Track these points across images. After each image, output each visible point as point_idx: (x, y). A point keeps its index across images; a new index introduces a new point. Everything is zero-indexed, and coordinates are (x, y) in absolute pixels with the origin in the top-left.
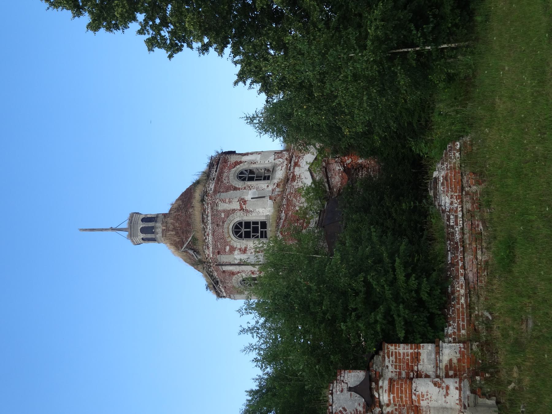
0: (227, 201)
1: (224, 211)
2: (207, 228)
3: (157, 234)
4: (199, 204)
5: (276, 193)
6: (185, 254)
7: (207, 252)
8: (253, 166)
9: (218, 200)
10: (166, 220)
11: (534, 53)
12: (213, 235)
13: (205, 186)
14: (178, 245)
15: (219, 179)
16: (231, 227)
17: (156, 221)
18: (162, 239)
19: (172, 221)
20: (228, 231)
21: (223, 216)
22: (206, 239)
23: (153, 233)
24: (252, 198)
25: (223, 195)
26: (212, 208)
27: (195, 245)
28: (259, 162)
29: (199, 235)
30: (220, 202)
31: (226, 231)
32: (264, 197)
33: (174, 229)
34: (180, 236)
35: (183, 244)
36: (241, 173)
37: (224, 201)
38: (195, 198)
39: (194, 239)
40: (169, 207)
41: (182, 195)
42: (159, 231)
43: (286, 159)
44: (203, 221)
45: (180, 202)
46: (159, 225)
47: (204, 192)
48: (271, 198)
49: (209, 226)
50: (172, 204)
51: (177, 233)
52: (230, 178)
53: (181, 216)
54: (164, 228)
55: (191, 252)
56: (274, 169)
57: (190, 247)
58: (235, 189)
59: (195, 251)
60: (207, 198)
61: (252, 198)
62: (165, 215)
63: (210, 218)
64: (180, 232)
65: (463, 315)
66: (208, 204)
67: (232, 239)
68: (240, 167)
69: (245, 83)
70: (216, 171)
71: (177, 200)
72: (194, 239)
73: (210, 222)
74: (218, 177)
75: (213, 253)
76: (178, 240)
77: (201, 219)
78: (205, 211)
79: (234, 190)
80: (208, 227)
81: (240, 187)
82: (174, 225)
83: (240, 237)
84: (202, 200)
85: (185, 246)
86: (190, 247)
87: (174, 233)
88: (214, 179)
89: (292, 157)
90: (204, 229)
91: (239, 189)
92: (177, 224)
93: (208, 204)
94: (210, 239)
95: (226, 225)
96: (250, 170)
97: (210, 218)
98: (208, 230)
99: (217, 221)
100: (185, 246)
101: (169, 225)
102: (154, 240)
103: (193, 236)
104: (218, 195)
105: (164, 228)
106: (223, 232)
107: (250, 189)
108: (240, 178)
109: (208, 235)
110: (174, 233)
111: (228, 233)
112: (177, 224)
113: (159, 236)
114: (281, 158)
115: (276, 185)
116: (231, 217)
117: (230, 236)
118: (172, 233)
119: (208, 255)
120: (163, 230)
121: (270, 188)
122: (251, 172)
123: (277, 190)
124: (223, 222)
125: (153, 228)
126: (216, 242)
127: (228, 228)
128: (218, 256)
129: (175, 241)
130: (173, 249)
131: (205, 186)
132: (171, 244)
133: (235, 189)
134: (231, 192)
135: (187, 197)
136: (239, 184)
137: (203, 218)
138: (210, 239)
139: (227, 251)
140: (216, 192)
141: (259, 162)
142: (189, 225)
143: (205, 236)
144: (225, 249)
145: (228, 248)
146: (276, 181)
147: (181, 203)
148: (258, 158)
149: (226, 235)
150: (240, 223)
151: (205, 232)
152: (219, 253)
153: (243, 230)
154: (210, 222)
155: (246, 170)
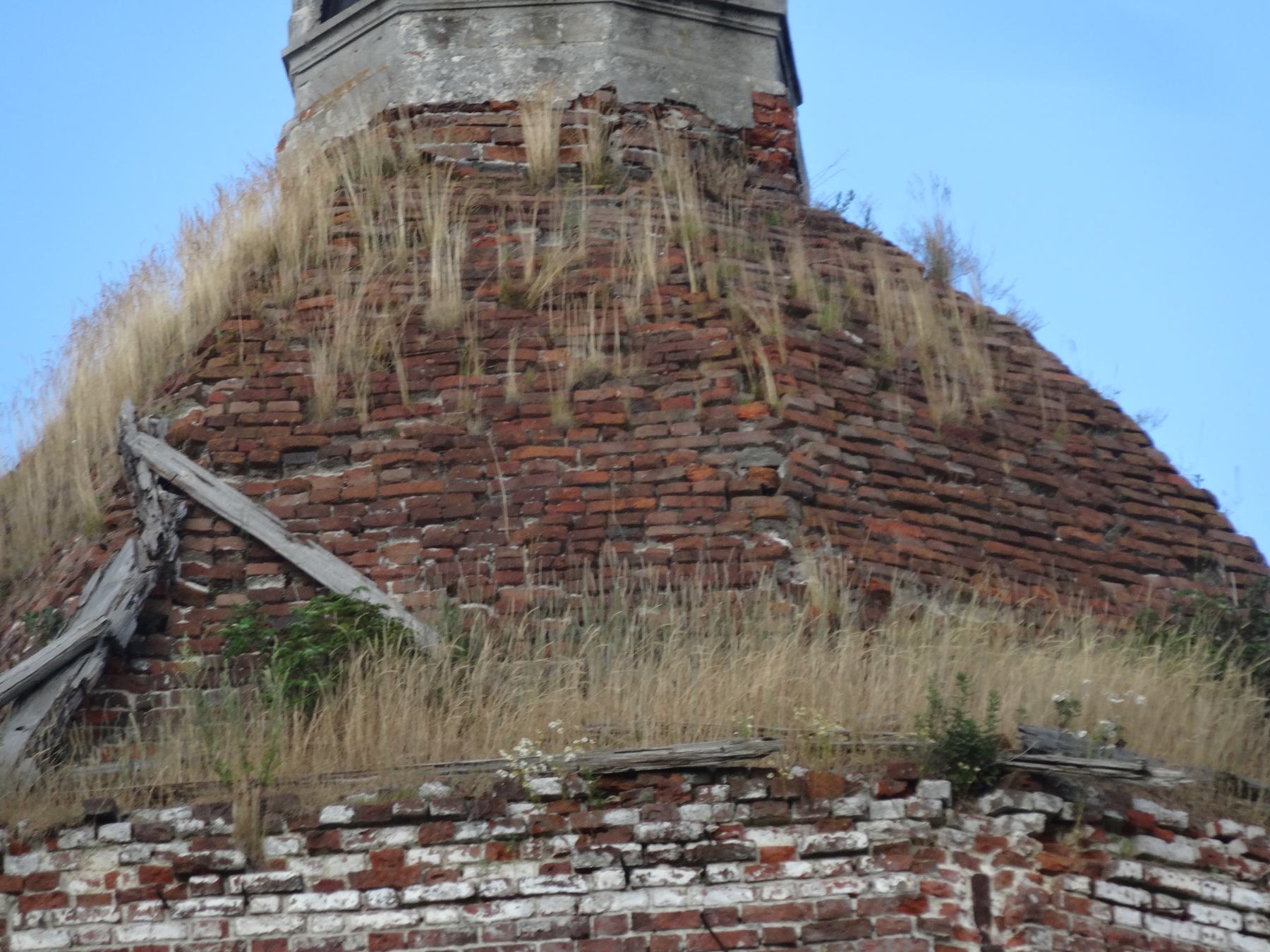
2: (504, 850)
4: (915, 701)
10: (672, 166)
13: (1235, 790)
14: (237, 375)
18: (354, 118)
19: (649, 263)
22: (321, 841)
27: (238, 657)
29: (385, 721)
33: (510, 308)
34: (383, 398)
35: (257, 467)
38: (1036, 628)
39: (318, 648)
40: (896, 221)
41: (1098, 418)
44: (614, 784)
45: (965, 389)
47: (1119, 788)
50: (938, 269)
51: (432, 354)
53: (717, 417)
54: (539, 137)
55: (108, 602)
57: (189, 579)
59: (129, 659)
60: (1017, 830)
62: (765, 145)
63: (668, 890)
64: (457, 405)
66: (913, 852)
69: (42, 554)
71: (1010, 343)
72: (318, 648)
73: (607, 894)
76: (320, 372)
77: (653, 749)
78: (795, 801)
80: (525, 874)
82: (574, 295)
84: (975, 764)
85: (222, 495)
86: (189, 579)
87: (445, 300)
90: (490, 806)
92: (581, 353)
93: (913, 852)
97: (668, 890)
98: (463, 863)
100: (222, 495)
101: (581, 209)
103: (367, 620)
105: (539, 137)
109: (388, 871)
110: (445, 300)
112: (581, 353)
118: (444, 273)
120: (495, 121)
129: (311, 314)
130: (183, 294)
131: (1235, 790)
132: (261, 266)
135: (250, 496)
137: (667, 780)
142: (574, 542)
143: (372, 819)
147: (946, 406)
151: (434, 827)
154: (607, 894)
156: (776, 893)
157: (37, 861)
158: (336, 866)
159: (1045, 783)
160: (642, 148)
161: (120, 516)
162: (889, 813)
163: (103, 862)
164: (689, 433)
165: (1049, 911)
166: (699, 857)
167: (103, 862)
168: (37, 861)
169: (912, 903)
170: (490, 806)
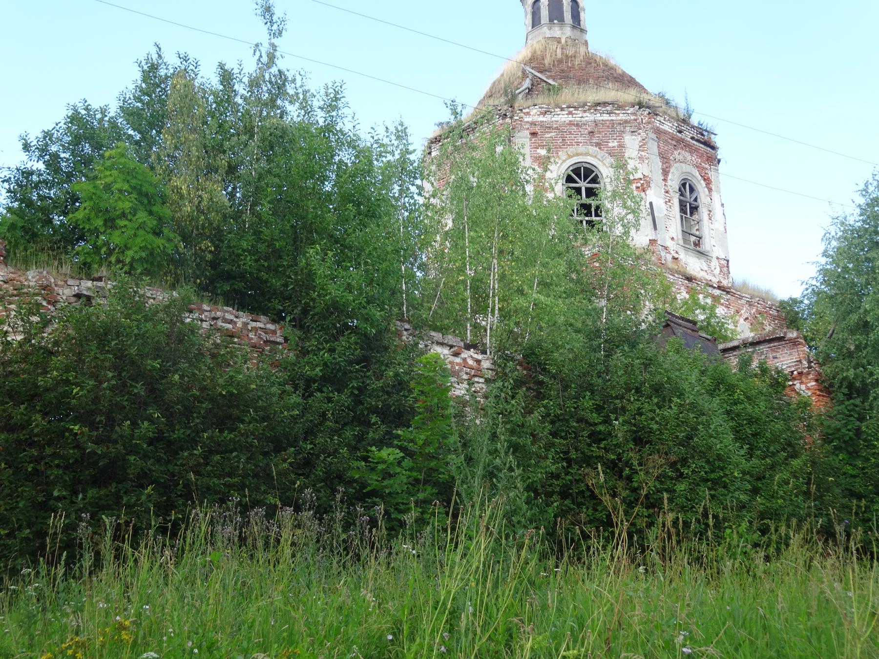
0: (643, 153)
1: (621, 146)
2: (585, 111)
3: (550, 29)
5: (663, 254)
6: (520, 74)
7: (534, 111)
8: (703, 212)
9: (643, 134)
11: (35, 452)
12: (571, 124)
15: (680, 143)
16: (589, 159)
17: (574, 27)
20: (581, 154)
21: (610, 145)
22: (562, 109)
23: (551, 20)
24: (651, 204)
25: (653, 147)
26: (626, 122)
28: (712, 226)
30: (639, 138)
31: (581, 149)
32: (655, 228)
36: (692, 190)
37: (642, 148)
42: (556, 32)
43: (719, 282)
44: (599, 104)
46: (568, 31)
48: (653, 242)
49: (589, 117)
52: (683, 165)
55: (527, 83)
56: (702, 254)
58: (665, 173)
61: (651, 204)
63: (606, 117)
64: (564, 66)
65: (480, 612)
66: (634, 114)
67: (564, 161)
68: (701, 186)
70: (692, 138)
73: (598, 117)
74: (683, 140)
75: (533, 124)
78: (620, 107)
79: (663, 170)
81: (669, 183)
83: (569, 179)
87: (559, 56)
88: (680, 132)
89: (728, 293)
91: (665, 180)
93: (634, 114)
94: (563, 117)
95: (593, 149)
96: (696, 208)
97: (606, 117)
99: (600, 132)
102: (536, 21)
104: (654, 136)
106: (578, 144)
107: (666, 202)
108: (684, 185)
109: (570, 113)
111: (577, 155)
113: (545, 31)
114: (721, 271)
115: (676, 256)
116: (610, 160)
117: (570, 157)
119: (528, 114)
121: (669, 244)
122: (694, 209)
123: (669, 257)
124: (598, 145)
125: (562, 20)
126: (557, 128)
127: (587, 154)
128: (527, 133)
133: (665, 173)
134: (660, 164)
136: (674, 182)
137: (605, 104)
138: (563, 117)
139: (539, 151)
140: (659, 132)
141: (712, 226)
143: (568, 107)
144: (543, 147)
145: (543, 152)
146: (682, 256)
148: (718, 225)
149: (571, 150)
150: (595, 180)
151: (576, 108)
152: (534, 134)
153: (583, 185)
154: (598, 117)
155: (696, 200)
156: (619, 118)
157: (527, 110)
158: (564, 113)
159: (649, 107)
160: (229, 407)
161: (525, 75)
162: (632, 109)
163: (535, 111)
164: (593, 71)
165: (437, 359)
166: (610, 113)
167: (535, 111)
168: (527, 110)
169: (636, 120)
170: (585, 104)
